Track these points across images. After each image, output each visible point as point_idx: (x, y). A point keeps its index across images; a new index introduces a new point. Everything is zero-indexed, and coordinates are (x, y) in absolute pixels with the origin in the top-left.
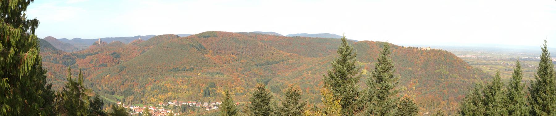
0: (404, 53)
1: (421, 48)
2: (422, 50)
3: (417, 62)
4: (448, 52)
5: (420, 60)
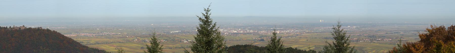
4: (50, 31)
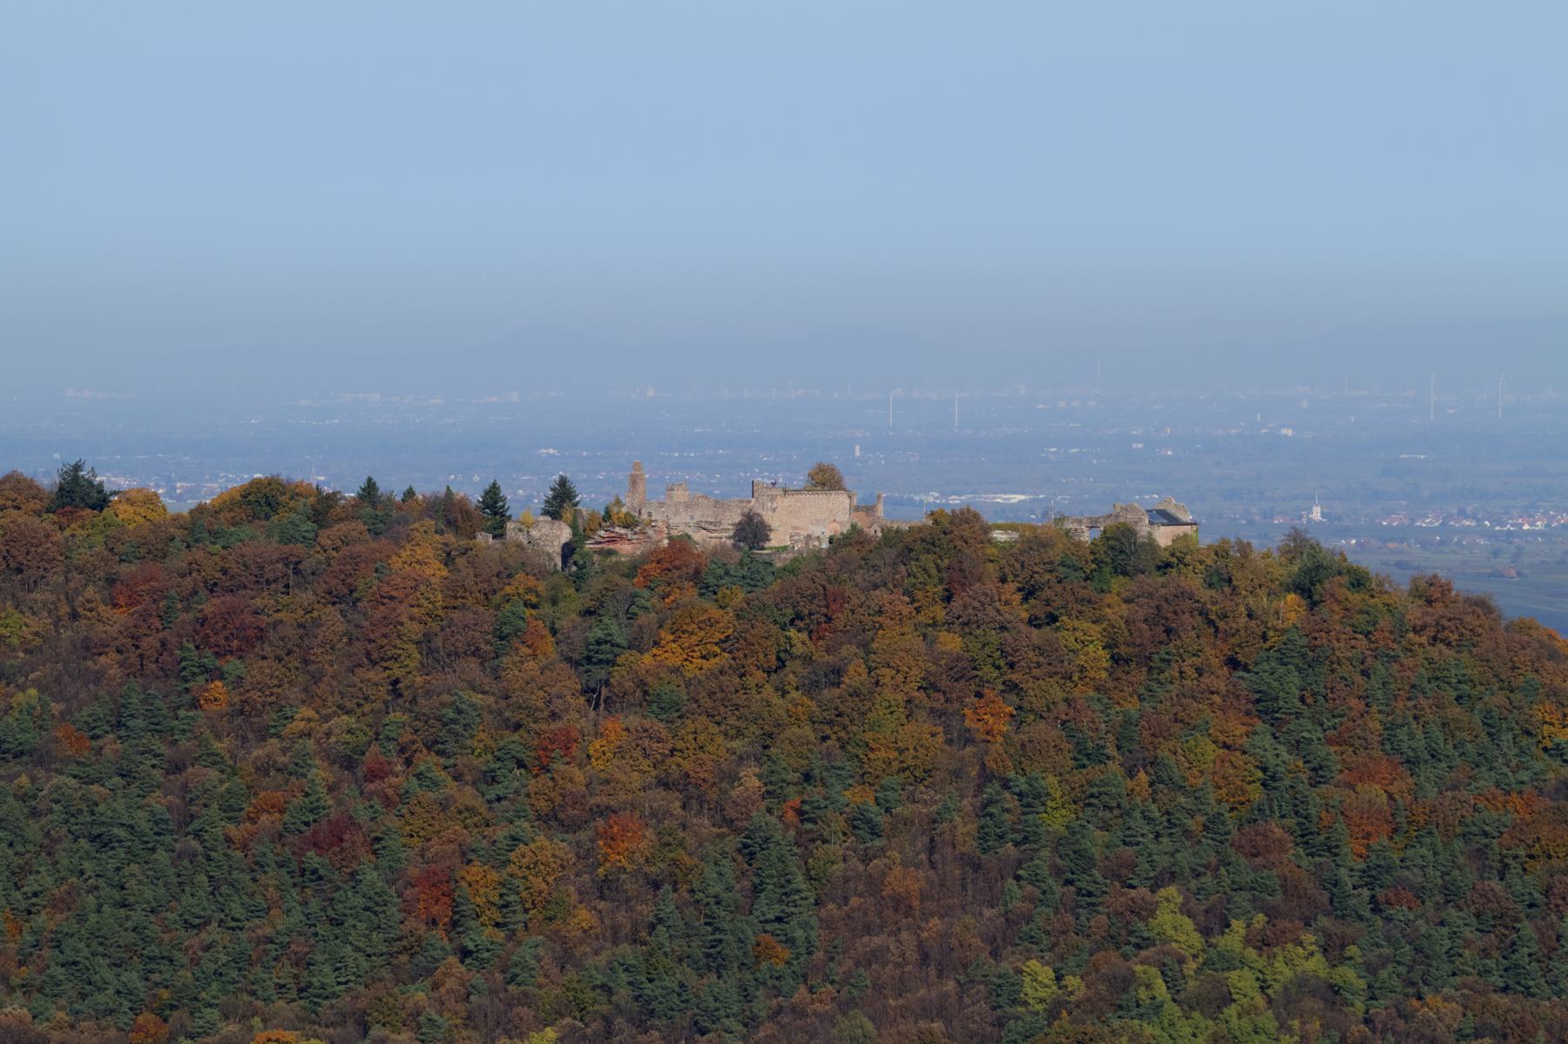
0: (108, 662)
1: (590, 500)
2: (627, 550)
3: (479, 883)
4: (1359, 581)
5: (551, 819)
